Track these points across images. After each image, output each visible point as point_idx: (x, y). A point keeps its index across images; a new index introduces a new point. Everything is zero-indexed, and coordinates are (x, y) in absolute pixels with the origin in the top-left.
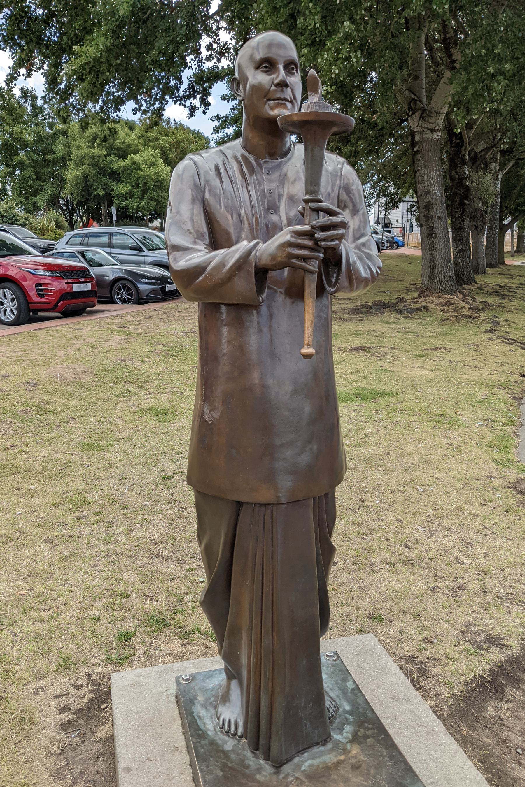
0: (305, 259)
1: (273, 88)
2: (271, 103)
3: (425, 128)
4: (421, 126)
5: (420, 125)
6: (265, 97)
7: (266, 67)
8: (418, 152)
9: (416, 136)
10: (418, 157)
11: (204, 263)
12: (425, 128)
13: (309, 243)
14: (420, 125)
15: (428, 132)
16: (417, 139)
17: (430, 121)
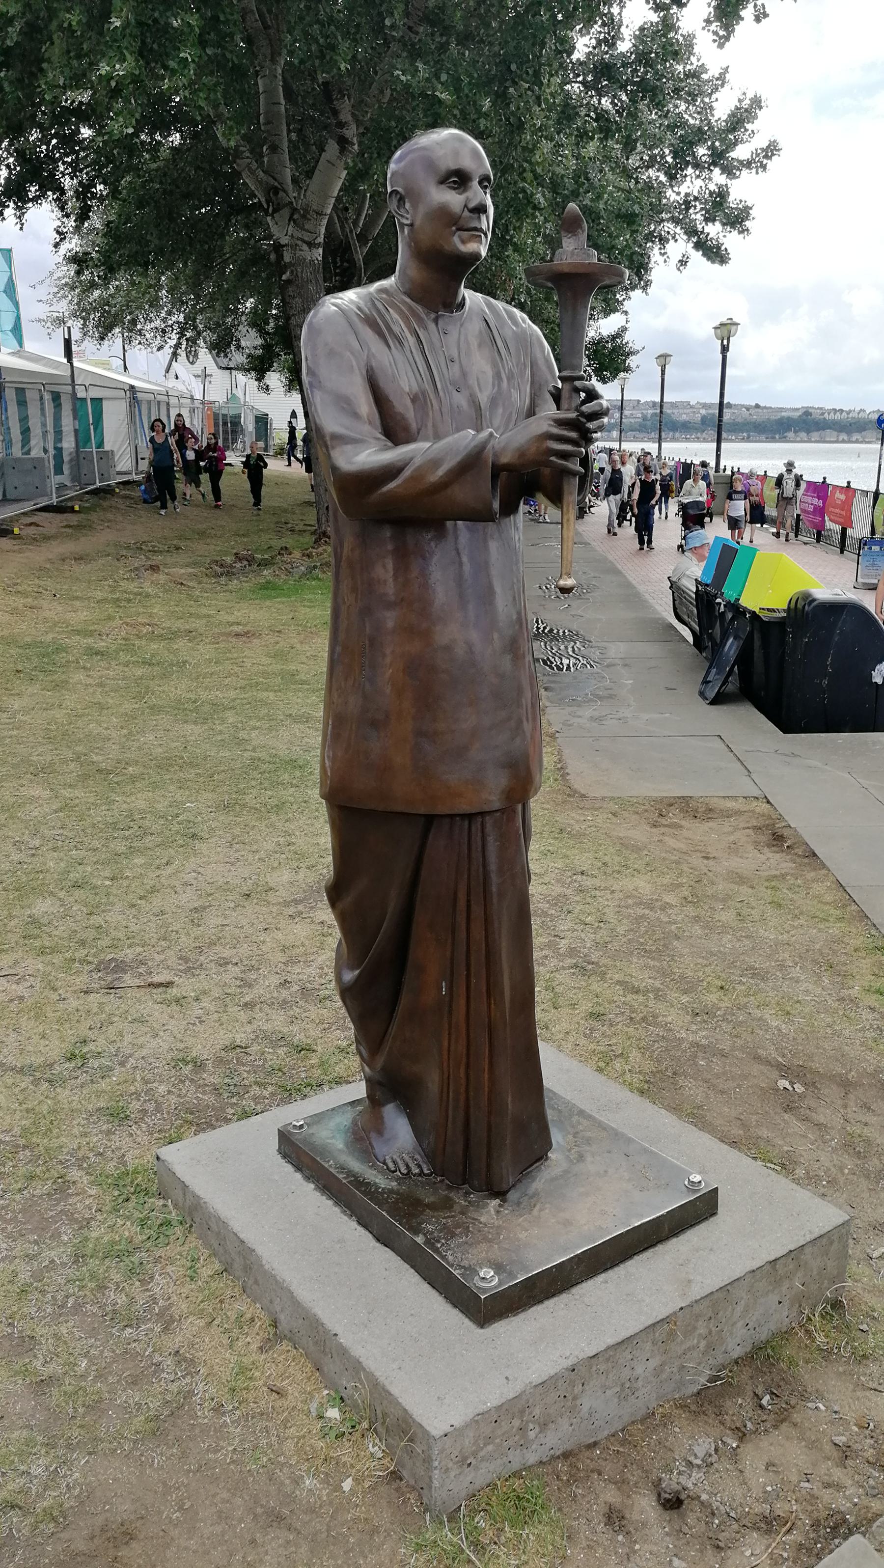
0: (565, 455)
1: (466, 213)
2: (465, 234)
3: (298, 239)
4: (292, 236)
5: (289, 233)
6: (454, 225)
7: (454, 182)
8: (289, 282)
9: (285, 253)
10: (291, 290)
11: (398, 461)
12: (298, 239)
13: (574, 435)
14: (289, 233)
15: (305, 247)
16: (287, 258)
17: (306, 227)
